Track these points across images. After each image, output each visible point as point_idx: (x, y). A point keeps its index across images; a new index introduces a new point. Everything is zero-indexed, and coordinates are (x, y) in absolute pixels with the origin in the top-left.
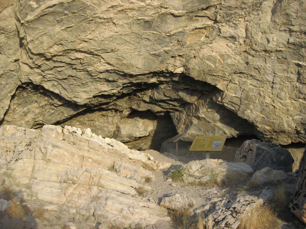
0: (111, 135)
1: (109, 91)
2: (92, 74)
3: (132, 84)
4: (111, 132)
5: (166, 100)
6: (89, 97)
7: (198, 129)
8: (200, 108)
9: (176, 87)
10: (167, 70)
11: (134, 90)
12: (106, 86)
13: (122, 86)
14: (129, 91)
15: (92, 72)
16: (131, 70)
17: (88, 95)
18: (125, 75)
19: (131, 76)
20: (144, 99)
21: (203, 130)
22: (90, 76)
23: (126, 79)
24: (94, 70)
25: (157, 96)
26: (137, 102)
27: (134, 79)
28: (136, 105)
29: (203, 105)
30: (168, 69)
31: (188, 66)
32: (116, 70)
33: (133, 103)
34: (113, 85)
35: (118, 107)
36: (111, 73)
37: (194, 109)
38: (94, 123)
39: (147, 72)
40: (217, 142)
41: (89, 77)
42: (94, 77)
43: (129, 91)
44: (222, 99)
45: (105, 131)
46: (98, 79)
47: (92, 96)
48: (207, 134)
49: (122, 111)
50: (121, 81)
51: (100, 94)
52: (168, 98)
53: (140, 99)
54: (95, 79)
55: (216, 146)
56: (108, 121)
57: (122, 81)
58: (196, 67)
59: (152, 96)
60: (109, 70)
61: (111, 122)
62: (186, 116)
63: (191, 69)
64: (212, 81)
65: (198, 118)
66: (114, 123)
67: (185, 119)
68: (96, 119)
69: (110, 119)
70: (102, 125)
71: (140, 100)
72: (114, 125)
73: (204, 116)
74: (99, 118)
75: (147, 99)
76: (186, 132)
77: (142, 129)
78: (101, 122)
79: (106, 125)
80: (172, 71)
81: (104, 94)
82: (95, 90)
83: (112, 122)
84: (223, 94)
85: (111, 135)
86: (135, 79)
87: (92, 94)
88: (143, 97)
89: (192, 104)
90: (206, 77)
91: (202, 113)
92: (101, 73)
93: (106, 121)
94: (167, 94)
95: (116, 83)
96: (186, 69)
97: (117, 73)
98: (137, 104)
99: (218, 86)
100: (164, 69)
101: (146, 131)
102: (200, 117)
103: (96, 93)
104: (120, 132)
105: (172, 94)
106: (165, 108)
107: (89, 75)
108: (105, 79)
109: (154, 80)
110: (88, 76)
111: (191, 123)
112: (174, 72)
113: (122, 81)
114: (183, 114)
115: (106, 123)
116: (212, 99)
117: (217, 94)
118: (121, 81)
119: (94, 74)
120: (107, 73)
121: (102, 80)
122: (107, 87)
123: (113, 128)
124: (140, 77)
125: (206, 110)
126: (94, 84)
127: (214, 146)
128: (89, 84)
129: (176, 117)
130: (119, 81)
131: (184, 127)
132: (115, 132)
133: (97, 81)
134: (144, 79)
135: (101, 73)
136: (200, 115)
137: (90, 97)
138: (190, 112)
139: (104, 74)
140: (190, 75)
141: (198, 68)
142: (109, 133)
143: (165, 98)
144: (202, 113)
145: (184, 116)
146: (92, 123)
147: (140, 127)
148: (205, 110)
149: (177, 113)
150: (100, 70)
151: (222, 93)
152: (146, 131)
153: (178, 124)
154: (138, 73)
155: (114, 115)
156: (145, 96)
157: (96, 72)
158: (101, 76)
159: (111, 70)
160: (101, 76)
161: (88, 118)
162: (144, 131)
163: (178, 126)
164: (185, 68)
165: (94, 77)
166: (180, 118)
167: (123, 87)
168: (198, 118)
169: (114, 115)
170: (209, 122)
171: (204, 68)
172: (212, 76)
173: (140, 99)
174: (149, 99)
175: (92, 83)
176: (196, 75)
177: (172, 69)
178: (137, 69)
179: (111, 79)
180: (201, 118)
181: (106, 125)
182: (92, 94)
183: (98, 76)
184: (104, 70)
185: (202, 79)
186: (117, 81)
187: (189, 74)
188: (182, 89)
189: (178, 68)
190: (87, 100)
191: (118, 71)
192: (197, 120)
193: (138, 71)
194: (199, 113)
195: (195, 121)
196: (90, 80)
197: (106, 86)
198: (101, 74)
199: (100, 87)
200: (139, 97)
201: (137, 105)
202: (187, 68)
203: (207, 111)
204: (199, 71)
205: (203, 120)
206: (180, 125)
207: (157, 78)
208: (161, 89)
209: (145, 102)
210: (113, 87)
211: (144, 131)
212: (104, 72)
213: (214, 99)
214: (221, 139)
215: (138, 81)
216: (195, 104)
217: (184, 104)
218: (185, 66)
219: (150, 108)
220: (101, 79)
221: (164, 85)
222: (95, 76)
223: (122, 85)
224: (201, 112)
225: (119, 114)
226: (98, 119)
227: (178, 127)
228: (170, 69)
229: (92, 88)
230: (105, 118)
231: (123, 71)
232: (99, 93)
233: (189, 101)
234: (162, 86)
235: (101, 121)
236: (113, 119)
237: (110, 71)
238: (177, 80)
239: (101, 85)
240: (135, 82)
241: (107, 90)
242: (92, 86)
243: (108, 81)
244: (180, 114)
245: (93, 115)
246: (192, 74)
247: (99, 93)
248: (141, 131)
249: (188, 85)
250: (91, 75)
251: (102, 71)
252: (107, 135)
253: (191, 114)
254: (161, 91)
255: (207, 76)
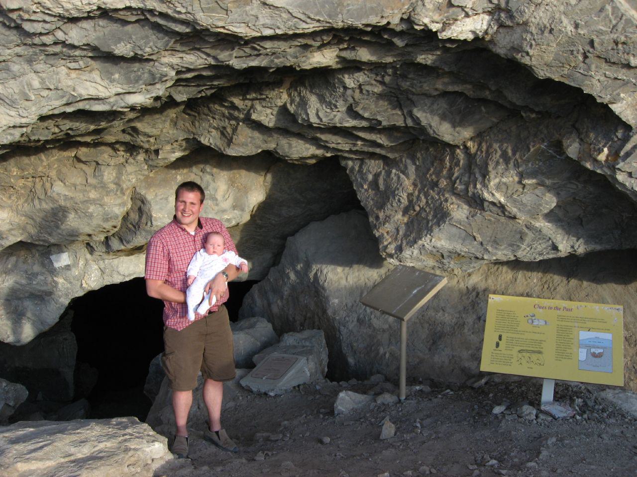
0: (115, 227)
1: (112, 100)
2: (27, 27)
3: (221, 70)
4: (117, 217)
5: (354, 128)
6: (19, 121)
7: (464, 234)
8: (490, 168)
9: (412, 85)
10: (408, 21)
11: (220, 89)
12: (98, 79)
13: (176, 78)
14: (200, 92)
15: (26, 17)
16: (234, 16)
17: (13, 113)
18: (196, 36)
19: (231, 41)
20: (254, 117)
21: (479, 238)
22: (15, 32)
23: (199, 50)
24: (34, 8)
25: (316, 110)
26: (222, 124)
27: (235, 53)
28: (214, 133)
29: (504, 155)
30: (416, 18)
31: (522, 13)
32: (151, 11)
33: (205, 125)
34: (133, 75)
35: (142, 138)
36: (125, 23)
37: (457, 164)
38: (48, 185)
39: (311, 27)
40: (592, 335)
41: (13, 36)
42: (37, 40)
43: (200, 92)
44: (615, 155)
45: (91, 216)
46: (58, 49)
47: (33, 118)
48: (490, 249)
49: (157, 152)
50: (175, 60)
51: (69, 110)
52: (364, 124)
53: (236, 113)
54: (44, 45)
55: (594, 355)
56: (102, 182)
57: (173, 61)
58: (565, 21)
59: (292, 109)
60: (116, 10)
61: (112, 186)
62: (415, 185)
63: (533, 29)
64: (605, 88)
65: (477, 203)
66: (124, 186)
67: (410, 195)
68: (53, 174)
69: (109, 175)
70: (80, 197)
71: (237, 119)
72: (124, 194)
73: (502, 200)
74: (64, 170)
75: (266, 116)
76: (415, 242)
77: (227, 204)
78: (75, 185)
79: (93, 195)
80: (434, 27)
81: (87, 107)
82: (45, 93)
83: (118, 184)
84: (626, 139)
85: (115, 227)
86: (241, 53)
87: (34, 109)
88: (252, 107)
89: (453, 147)
90: (589, 69)
91: (498, 187)
92: (74, 20)
93: (91, 180)
94: (364, 109)
95: (148, 66)
96: (501, 26)
97: (157, 27)
98: (223, 132)
99: (616, 108)
100: (395, 21)
101: (243, 210)
102: (483, 200)
103: (55, 105)
104: (150, 218)
105: (385, 111)
106: (327, 148)
107: (9, 27)
108: (95, 49)
109: (325, 58)
110: (8, 33)
111: (441, 216)
112: (443, 36)
113: (173, 61)
114: (403, 173)
115: (95, 187)
116: (559, 147)
117: (592, 135)
118: (175, 60)
119: (38, 28)
120: (102, 22)
121: (77, 53)
122: (105, 83)
123: (123, 204)
124: (268, 44)
125: (517, 179)
126: (40, 67)
127: (583, 354)
128: (15, 68)
129: (370, 177)
130: (165, 60)
131: (406, 220)
132: (126, 218)
133: (55, 54)
134: (289, 55)
135: (74, 20)
136: (486, 195)
137: (24, 121)
138: (438, 174)
139: (85, 24)
140: (519, 56)
141: (570, 28)
142: (106, 220)
143: (350, 123)
144: (498, 187)
145: (407, 183)
146: (39, 186)
147: (219, 196)
148: (511, 178)
149: (374, 166)
150: (69, 6)
151: (620, 134)
152: (243, 210)
153: (381, 207)
154: (268, 32)
155: (122, 160)
156: (258, 107)
157: (48, 18)
158: (75, 35)
159: (128, 9)
160: (75, 35)
161: (23, 170)
162: (234, 207)
163: (381, 215)
164: (498, 20)
165: (37, 40)
166: (388, 187)
167: (178, 81)
168: (477, 203)
169: (122, 160)
170: (514, 218)
171: (600, 33)
172: (614, 68)
173: (236, 113)
174: (273, 118)
175: (30, 61)
176: (549, 58)
177: (436, 17)
178: (266, 11)
179: (121, 49)
180: (486, 204)
181: (93, 195)
182: (34, 109)
183: (60, 35)
184: (88, 9)
185: (568, 76)
186: (154, 57)
187: (519, 49)
188: (436, 93)
189: (467, 15)
190: (12, 131)
191: (163, 15)
192: (466, 207)
193: (268, 22)
194: (485, 186)
195: (459, 211)
196: (18, 50)
197: (96, 75)
198: (69, 25)
199: (70, 83)
200: (234, 107)
201: (222, 134)
202: (509, 23)
203: (520, 182)
204: (571, 42)
205: (494, 209)
206: (388, 213)
207: (341, 50)
208: (345, 88)
209: (258, 126)
210: (129, 81)
211: (234, 207)
212: (89, 17)
213: (573, 149)
214: (603, 321)
215: (254, 63)
216: (466, 148)
217: (415, 140)
218: (508, 11)
219: (271, 146)
220: (73, 47)
221: (361, 77)
222: (41, 34)
223: (173, 73)
224: (493, 183)
225: (141, 157)
226: (59, 172)
227: (377, 218)
228: (426, 21)
229: (29, 85)
230: (89, 170)
231: (189, 17)
232: (68, 104)
233: (447, 138)
234: (349, 81)
235: (73, 181)
236: (120, 174)
237: (121, 15)
238: (429, 62)
239: (74, 75)
240: (237, 64)
241: (102, 93)
242: (33, 75)
243: (109, 58)
244: (389, 174)
245: (42, 161)
246: (531, 52)
247: (68, 104)
248: (224, 211)
249: (464, 82)
250: (18, 28)
251: (76, 14)
252: (99, 226)
253: (443, 183)
254: (344, 95)
255: (594, 62)
